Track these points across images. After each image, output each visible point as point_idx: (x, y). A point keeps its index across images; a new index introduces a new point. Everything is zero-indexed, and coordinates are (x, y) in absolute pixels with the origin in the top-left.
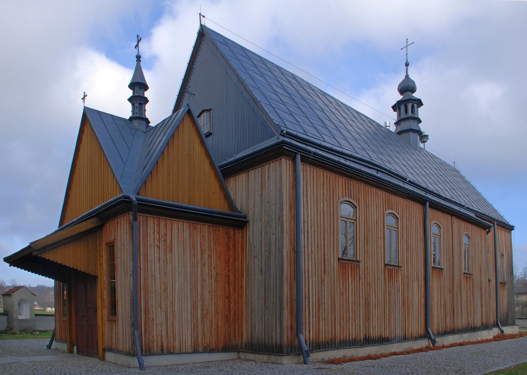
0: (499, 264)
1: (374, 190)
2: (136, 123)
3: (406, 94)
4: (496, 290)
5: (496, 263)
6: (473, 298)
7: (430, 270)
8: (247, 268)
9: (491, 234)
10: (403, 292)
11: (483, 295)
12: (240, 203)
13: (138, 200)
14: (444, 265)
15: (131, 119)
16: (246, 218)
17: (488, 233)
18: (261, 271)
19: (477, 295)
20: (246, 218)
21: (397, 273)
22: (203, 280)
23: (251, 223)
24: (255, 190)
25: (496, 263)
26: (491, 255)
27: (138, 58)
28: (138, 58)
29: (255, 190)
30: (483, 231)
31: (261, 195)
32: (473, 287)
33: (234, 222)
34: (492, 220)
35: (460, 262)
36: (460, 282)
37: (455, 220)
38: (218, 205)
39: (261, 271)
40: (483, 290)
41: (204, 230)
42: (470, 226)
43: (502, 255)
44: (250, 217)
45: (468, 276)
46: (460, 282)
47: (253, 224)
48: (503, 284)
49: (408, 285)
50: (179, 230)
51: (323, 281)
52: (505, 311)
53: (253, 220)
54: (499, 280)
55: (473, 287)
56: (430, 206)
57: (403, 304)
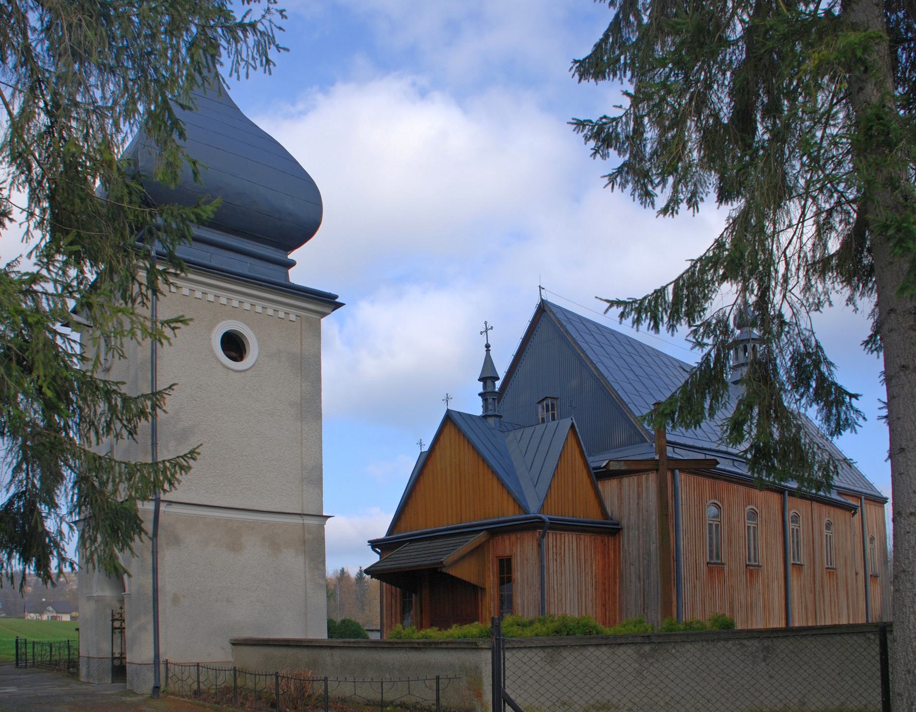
0: (868, 551)
1: (735, 486)
2: (491, 421)
3: (745, 329)
4: (866, 586)
5: (864, 551)
6: (838, 598)
7: (790, 568)
8: (621, 576)
9: (858, 516)
10: (763, 594)
11: (850, 593)
12: (611, 506)
13: (550, 519)
14: (804, 560)
15: (485, 417)
16: (618, 525)
17: (853, 515)
18: (639, 578)
19: (842, 594)
20: (618, 525)
21: (758, 573)
22: (586, 589)
23: (625, 530)
24: (629, 498)
25: (864, 551)
26: (858, 539)
27: (488, 346)
28: (488, 346)
29: (629, 498)
30: (848, 513)
31: (638, 504)
32: (837, 584)
33: (607, 530)
34: (857, 495)
35: (822, 556)
36: (822, 578)
37: (815, 505)
38: (594, 515)
39: (639, 578)
40: (850, 587)
41: (586, 539)
42: (832, 510)
43: (872, 539)
44: (624, 523)
45: (831, 571)
46: (822, 578)
47: (629, 532)
48: (875, 577)
49: (768, 586)
50: (569, 540)
51: (695, 587)
52: (878, 613)
53: (628, 528)
54: (869, 573)
55: (837, 584)
56: (789, 495)
57: (764, 607)
